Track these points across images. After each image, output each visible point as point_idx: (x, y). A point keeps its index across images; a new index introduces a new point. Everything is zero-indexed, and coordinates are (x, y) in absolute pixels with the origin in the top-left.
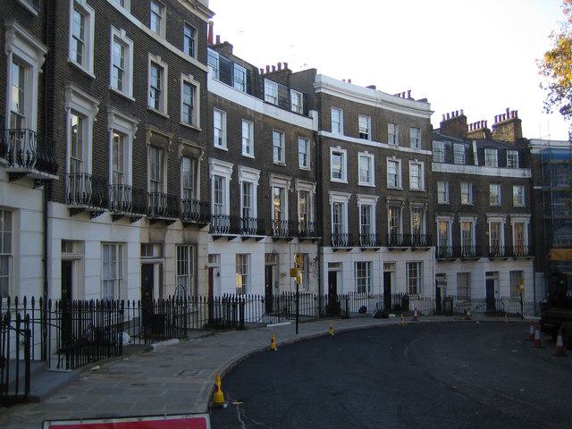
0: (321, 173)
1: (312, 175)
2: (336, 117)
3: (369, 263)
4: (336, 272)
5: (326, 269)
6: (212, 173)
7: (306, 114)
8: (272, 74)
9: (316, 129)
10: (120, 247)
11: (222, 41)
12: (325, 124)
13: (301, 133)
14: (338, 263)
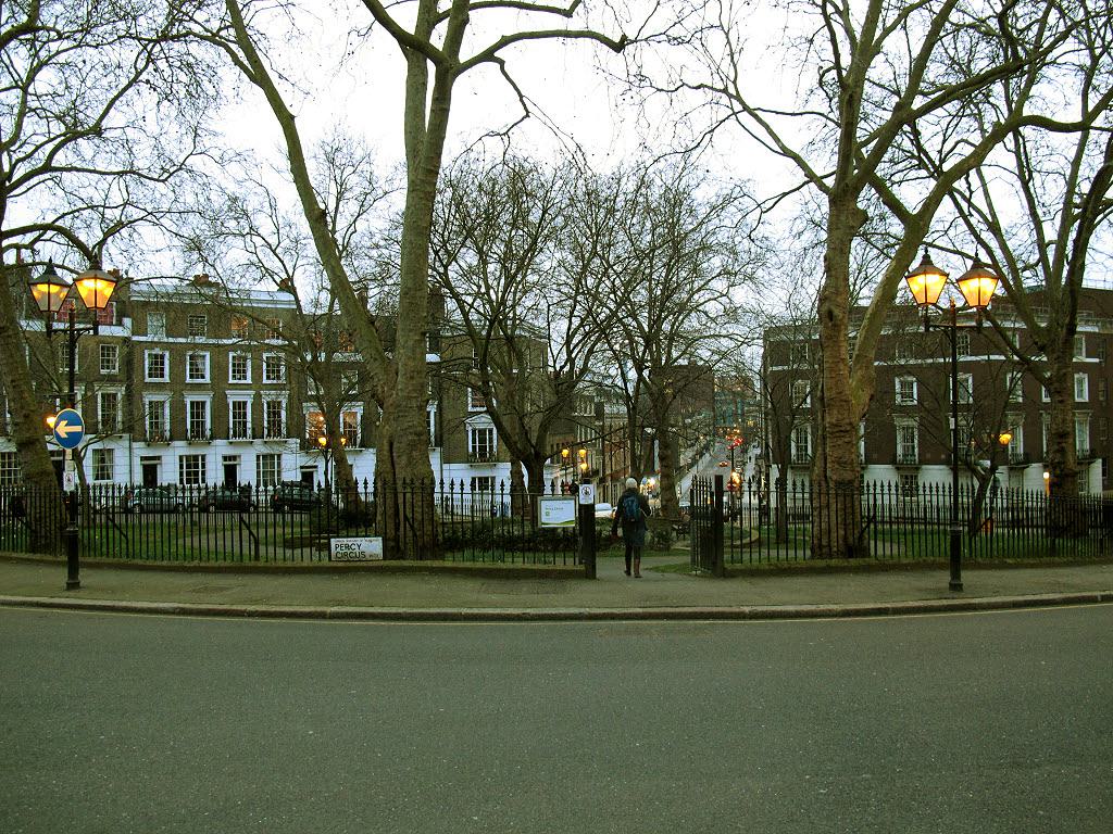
7: (120, 324)
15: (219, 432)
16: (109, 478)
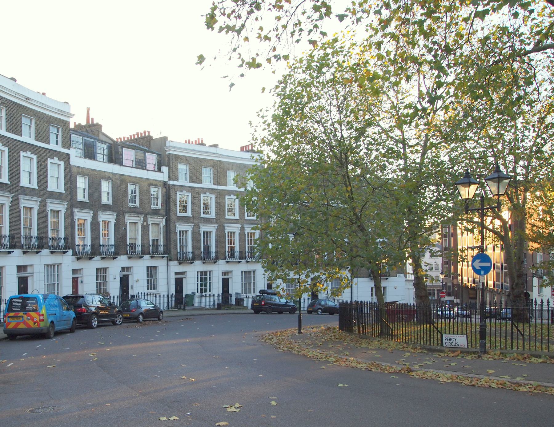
0: (169, 210)
1: (162, 212)
2: (183, 168)
3: (210, 272)
4: (182, 278)
5: (173, 277)
6: (22, 205)
7: (159, 170)
8: (136, 139)
9: (166, 179)
10: (58, 266)
11: (95, 123)
12: (173, 175)
13: (152, 183)
14: (184, 272)
15: (145, 251)
16: (154, 289)
